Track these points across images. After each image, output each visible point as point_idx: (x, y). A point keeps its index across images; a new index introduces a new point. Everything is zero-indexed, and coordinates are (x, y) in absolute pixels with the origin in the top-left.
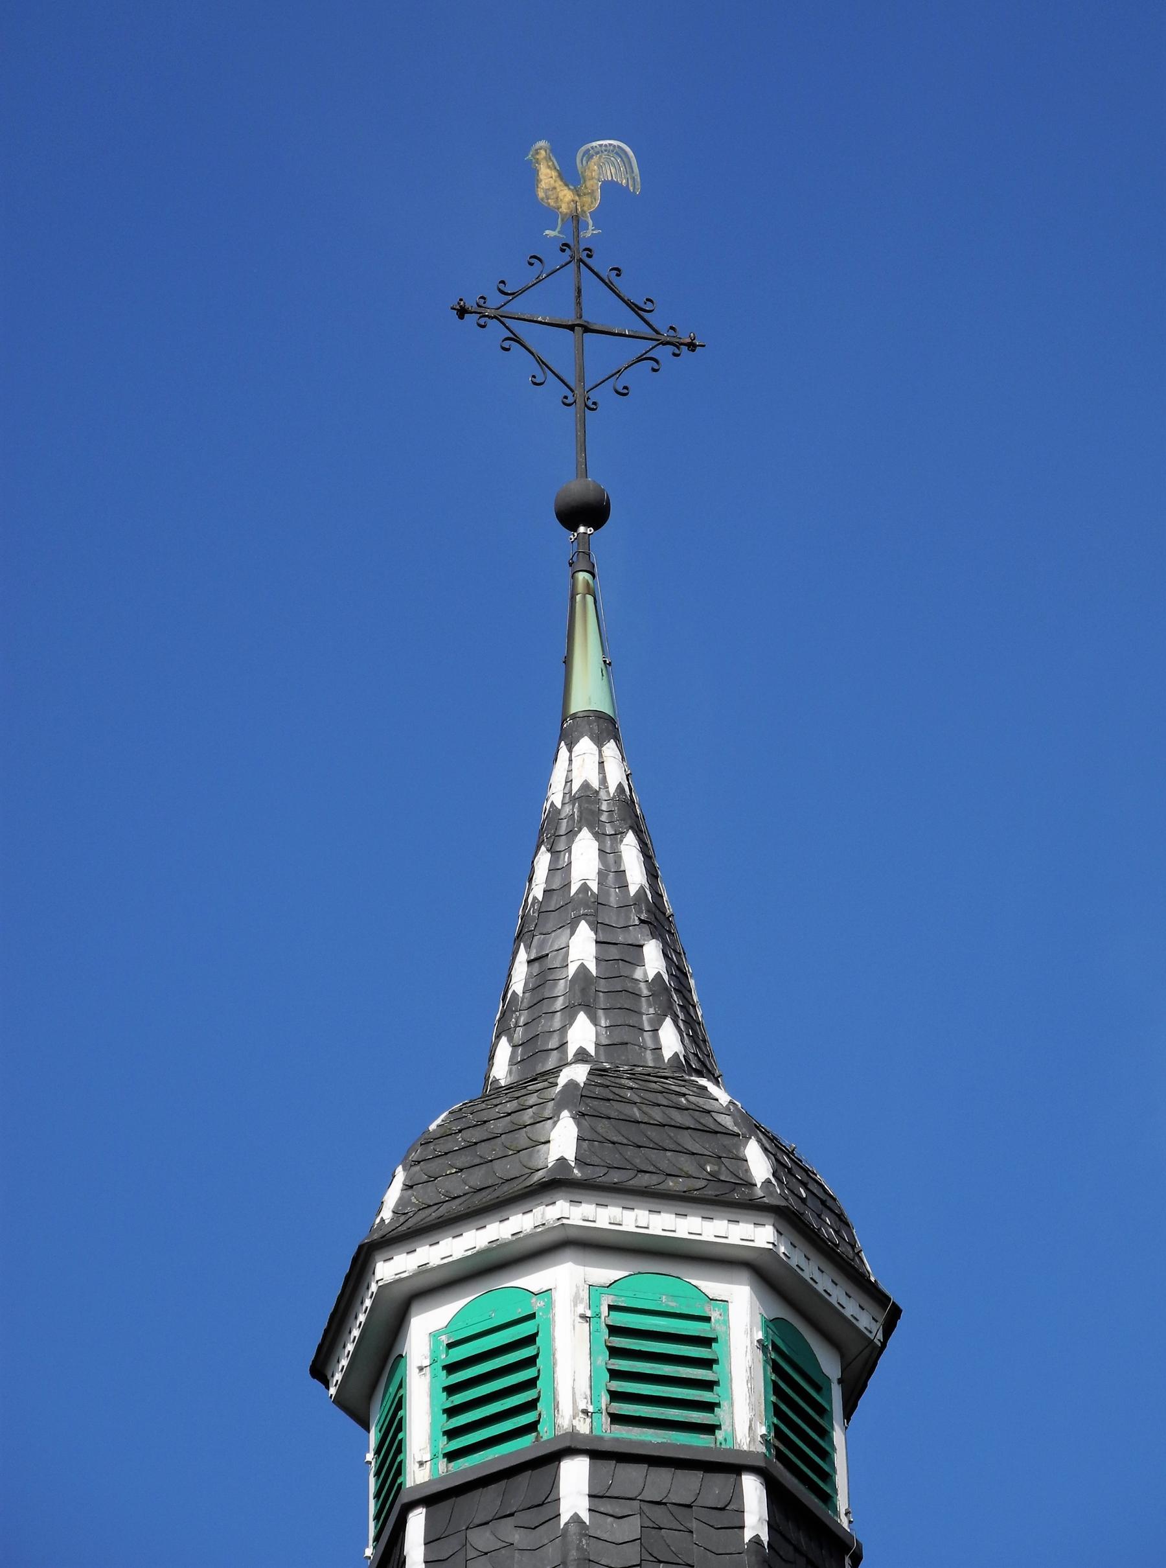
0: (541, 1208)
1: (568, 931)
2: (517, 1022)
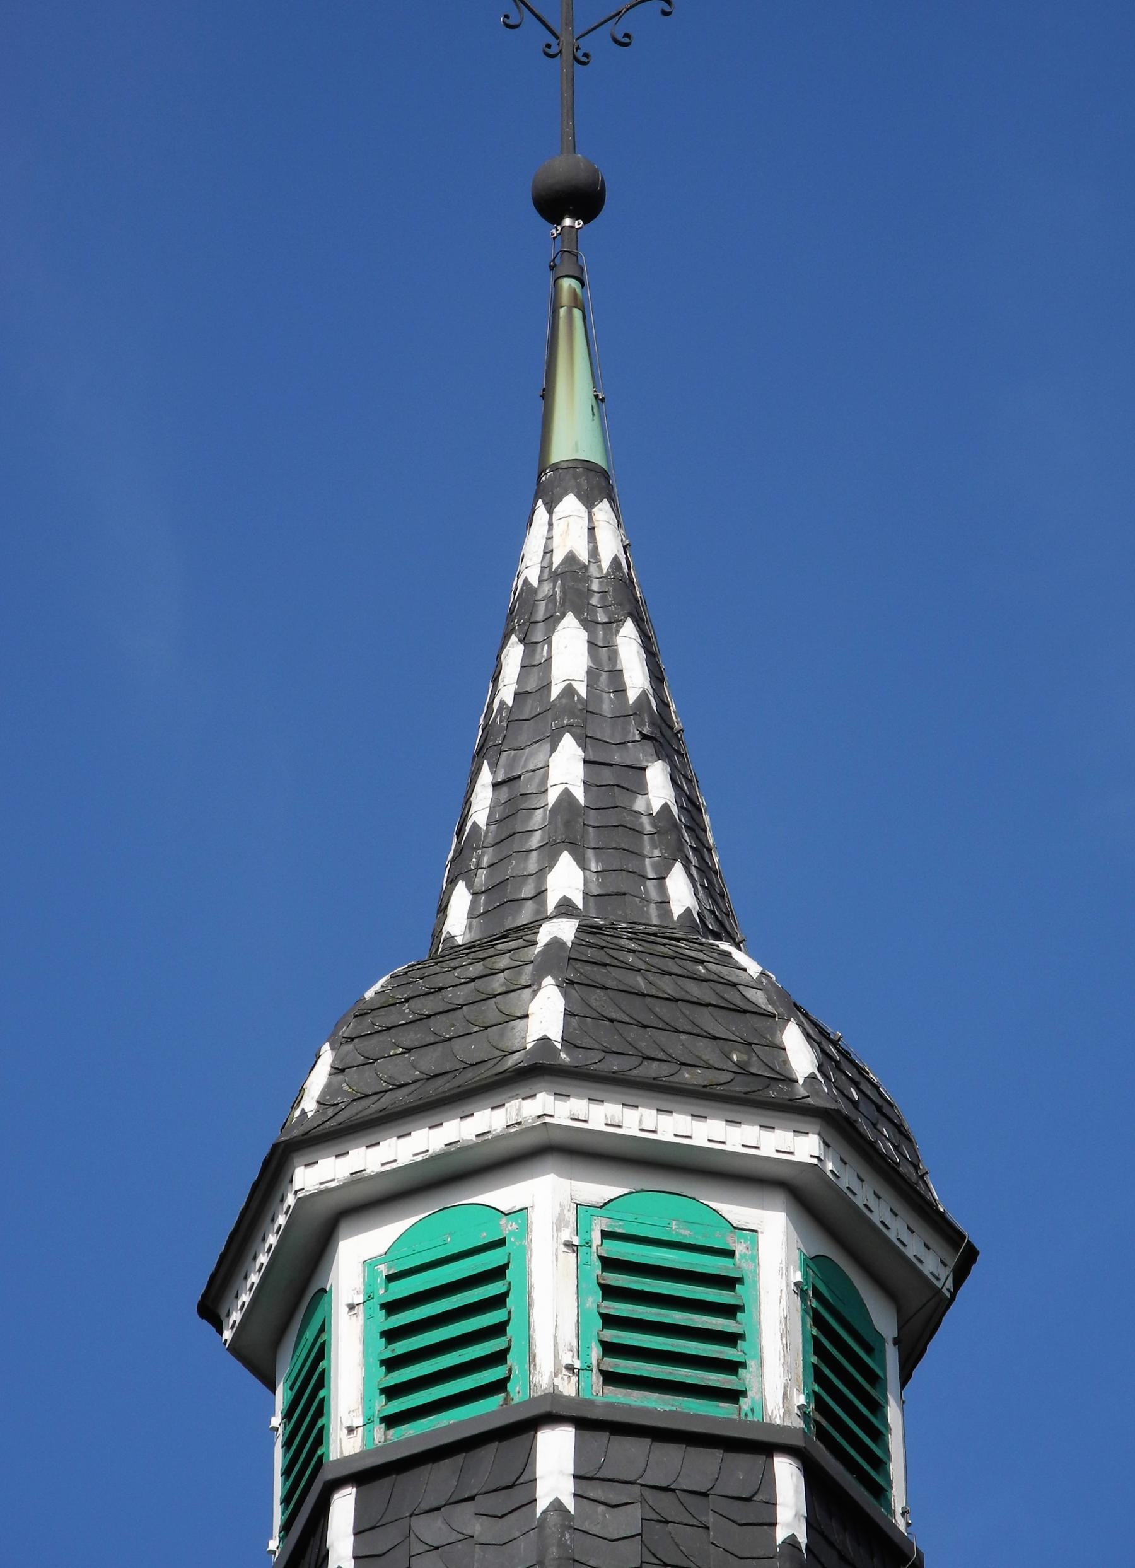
0: (516, 1103)
1: (548, 747)
2: (478, 863)
